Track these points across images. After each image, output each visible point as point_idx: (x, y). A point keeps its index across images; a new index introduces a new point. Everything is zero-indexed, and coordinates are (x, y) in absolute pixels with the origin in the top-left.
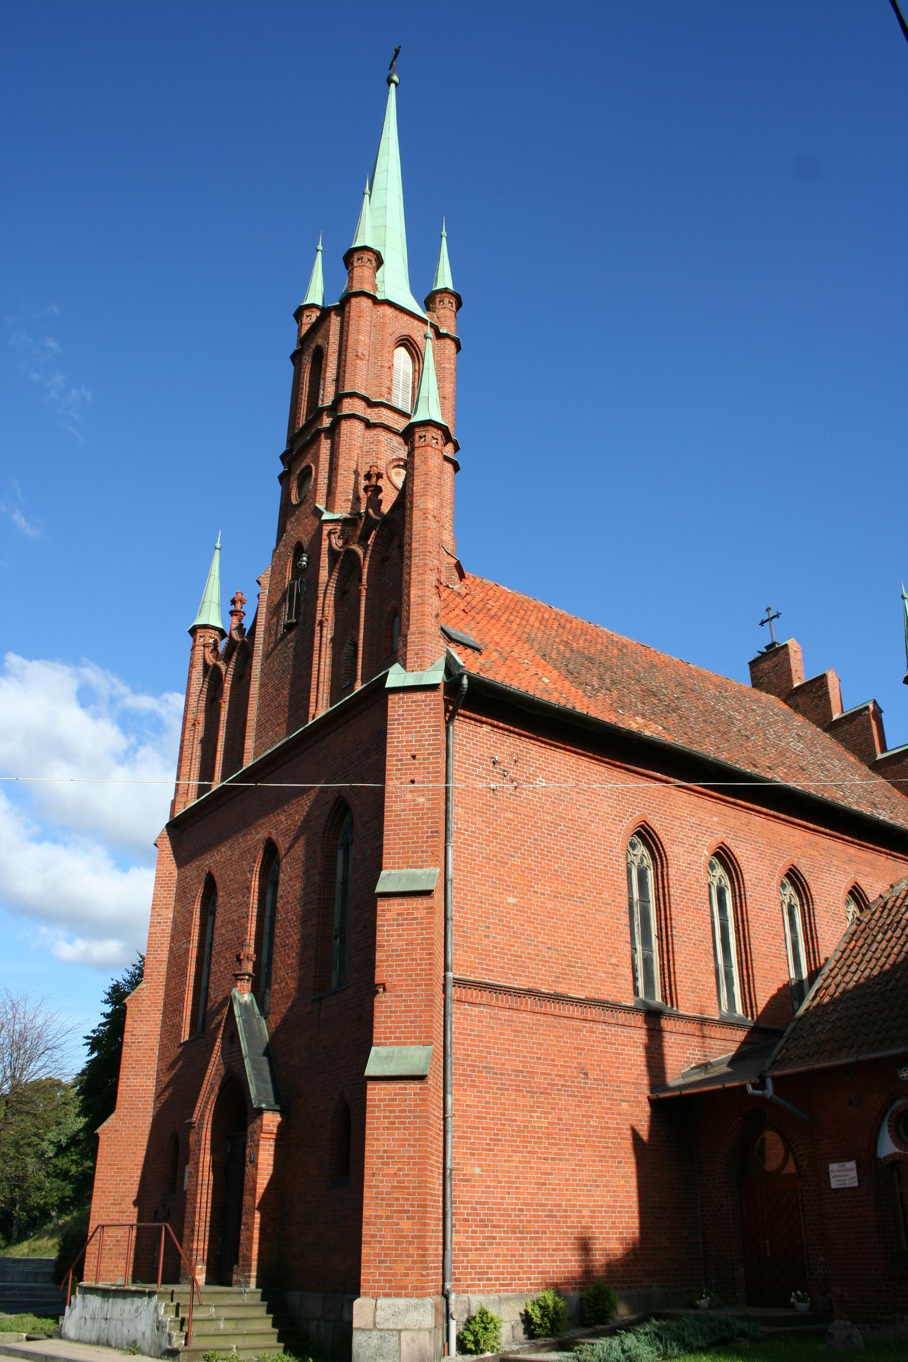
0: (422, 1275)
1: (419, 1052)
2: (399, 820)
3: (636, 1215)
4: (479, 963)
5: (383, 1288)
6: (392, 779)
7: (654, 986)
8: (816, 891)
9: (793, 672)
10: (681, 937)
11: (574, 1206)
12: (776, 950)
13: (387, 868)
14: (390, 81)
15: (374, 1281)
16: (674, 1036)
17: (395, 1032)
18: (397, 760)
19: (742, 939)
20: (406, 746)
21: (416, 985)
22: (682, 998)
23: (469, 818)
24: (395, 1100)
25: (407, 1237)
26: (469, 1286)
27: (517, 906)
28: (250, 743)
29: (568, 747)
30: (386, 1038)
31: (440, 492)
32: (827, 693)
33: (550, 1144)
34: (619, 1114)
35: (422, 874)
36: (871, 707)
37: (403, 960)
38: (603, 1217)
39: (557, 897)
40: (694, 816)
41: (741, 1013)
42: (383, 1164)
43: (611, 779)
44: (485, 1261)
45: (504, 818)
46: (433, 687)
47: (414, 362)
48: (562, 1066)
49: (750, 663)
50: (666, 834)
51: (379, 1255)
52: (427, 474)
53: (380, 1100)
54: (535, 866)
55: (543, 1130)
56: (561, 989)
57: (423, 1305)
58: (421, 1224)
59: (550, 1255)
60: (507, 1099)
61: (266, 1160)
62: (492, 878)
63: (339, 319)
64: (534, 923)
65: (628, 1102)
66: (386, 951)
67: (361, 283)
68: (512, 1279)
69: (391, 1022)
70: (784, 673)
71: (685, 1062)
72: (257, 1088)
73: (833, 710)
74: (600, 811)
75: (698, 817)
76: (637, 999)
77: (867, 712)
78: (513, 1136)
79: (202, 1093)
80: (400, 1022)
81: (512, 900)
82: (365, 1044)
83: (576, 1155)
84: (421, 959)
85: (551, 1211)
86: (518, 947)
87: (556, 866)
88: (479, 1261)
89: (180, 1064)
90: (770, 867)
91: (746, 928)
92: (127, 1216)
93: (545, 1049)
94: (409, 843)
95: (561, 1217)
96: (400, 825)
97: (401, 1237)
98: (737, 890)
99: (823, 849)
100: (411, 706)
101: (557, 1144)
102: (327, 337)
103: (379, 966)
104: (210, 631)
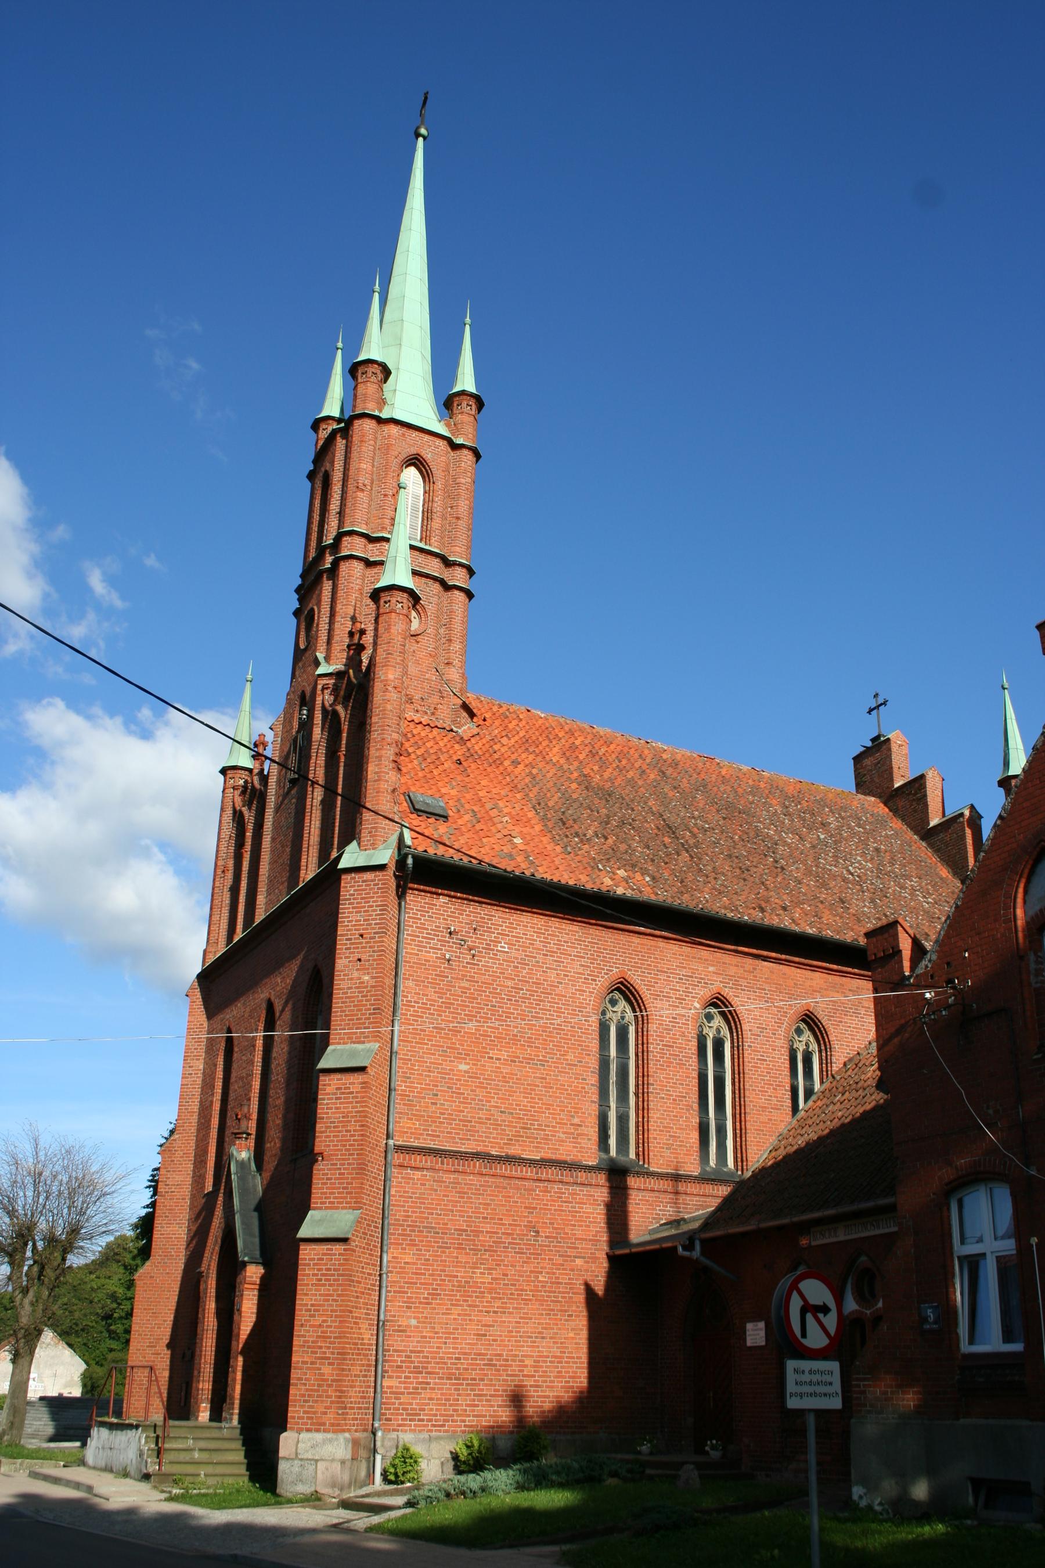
0: (338, 1414)
1: (348, 1216)
2: (346, 998)
3: (586, 1365)
4: (424, 1130)
5: (307, 1424)
6: (341, 958)
7: (629, 1143)
8: (836, 1036)
9: (895, 770)
10: (659, 1094)
11: (516, 1356)
12: (777, 1101)
13: (334, 1044)
14: (418, 135)
15: (299, 1418)
16: (641, 1194)
17: (329, 1198)
18: (347, 940)
19: (737, 1092)
20: (355, 925)
21: (350, 1155)
22: (654, 1155)
23: (419, 990)
24: (322, 1259)
25: (327, 1380)
26: (400, 1425)
27: (469, 1072)
28: (261, 899)
29: (534, 910)
30: (322, 1203)
31: (403, 661)
32: (925, 796)
33: (492, 1298)
34: (572, 1270)
35: (363, 1050)
36: (967, 813)
37: (339, 1132)
38: (547, 1367)
39: (515, 1062)
40: (685, 968)
41: (733, 1168)
42: (311, 1316)
43: (585, 937)
44: (417, 1404)
45: (459, 987)
46: (382, 867)
47: (424, 482)
48: (510, 1225)
49: (854, 759)
50: (647, 990)
51: (304, 1396)
52: (389, 643)
53: (310, 1259)
54: (491, 1032)
55: (486, 1285)
56: (512, 1151)
57: (337, 1439)
58: (340, 1369)
59: (487, 1401)
60: (448, 1257)
61: (250, 1308)
62: (442, 1046)
63: (344, 442)
64: (487, 1088)
65: (584, 1258)
66: (325, 1123)
67: (364, 401)
68: (445, 1421)
69: (327, 1188)
70: (886, 771)
71: (654, 1218)
72: (244, 1242)
73: (930, 815)
74: (570, 972)
75: (689, 968)
76: (604, 1156)
77: (961, 819)
78: (453, 1291)
79: (208, 1244)
80: (334, 1188)
81: (463, 1067)
82: (304, 1208)
83: (520, 1308)
84: (354, 1131)
85: (491, 1360)
86: (468, 1112)
87: (516, 1030)
88: (411, 1404)
89: (203, 1214)
90: (777, 1015)
91: (742, 1080)
92: (161, 1358)
93: (492, 1209)
94: (353, 1020)
95: (501, 1366)
96: (346, 1002)
97: (323, 1380)
98: (735, 1041)
99: (850, 990)
100: (362, 886)
101: (500, 1298)
102: (332, 463)
103: (318, 1137)
104: (240, 771)
